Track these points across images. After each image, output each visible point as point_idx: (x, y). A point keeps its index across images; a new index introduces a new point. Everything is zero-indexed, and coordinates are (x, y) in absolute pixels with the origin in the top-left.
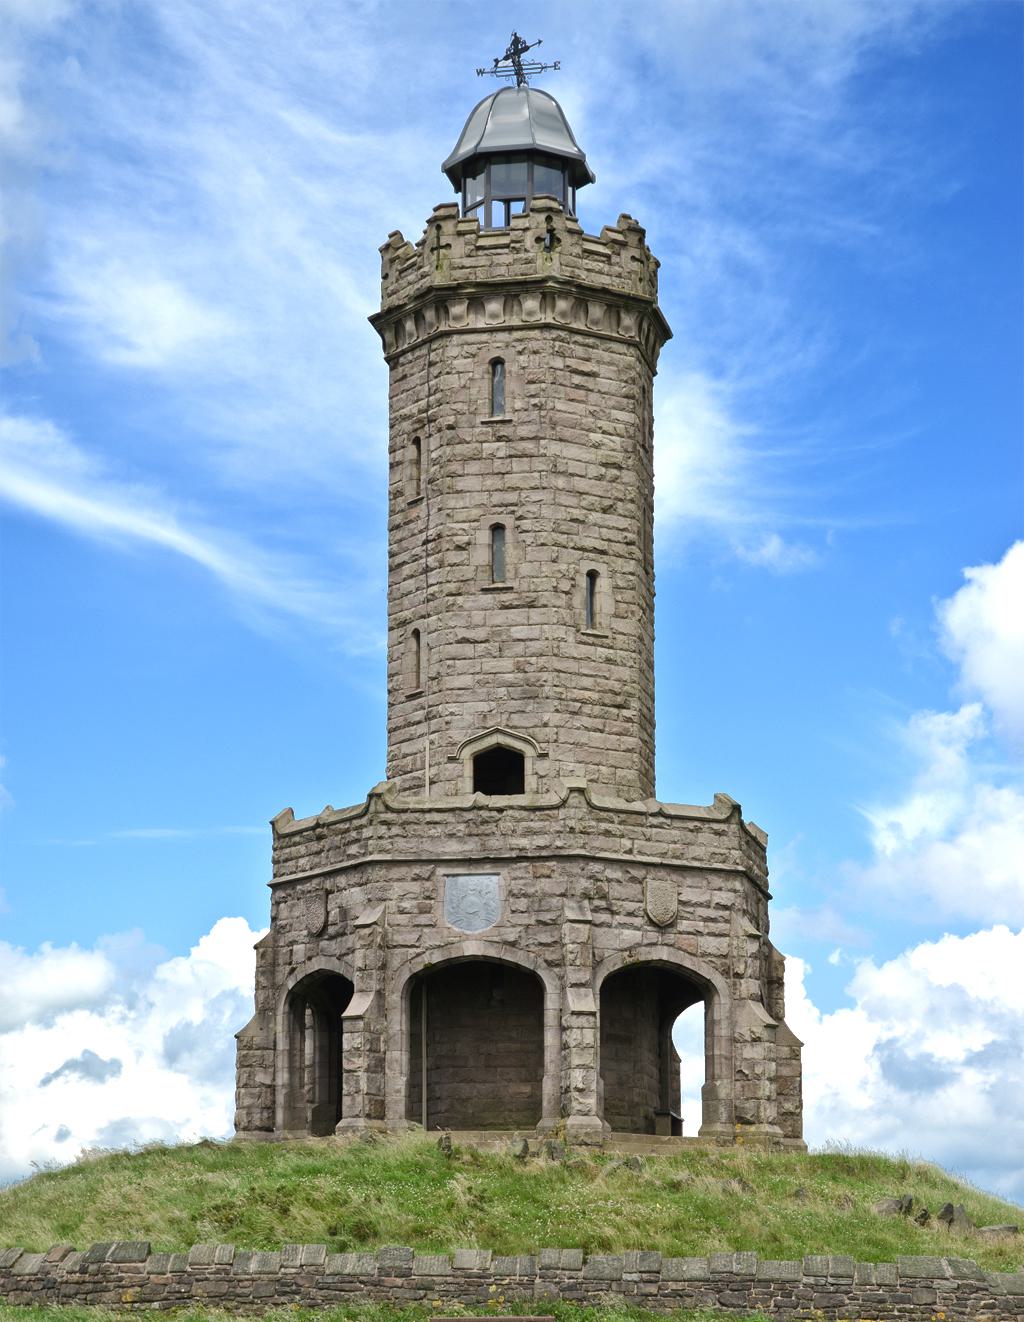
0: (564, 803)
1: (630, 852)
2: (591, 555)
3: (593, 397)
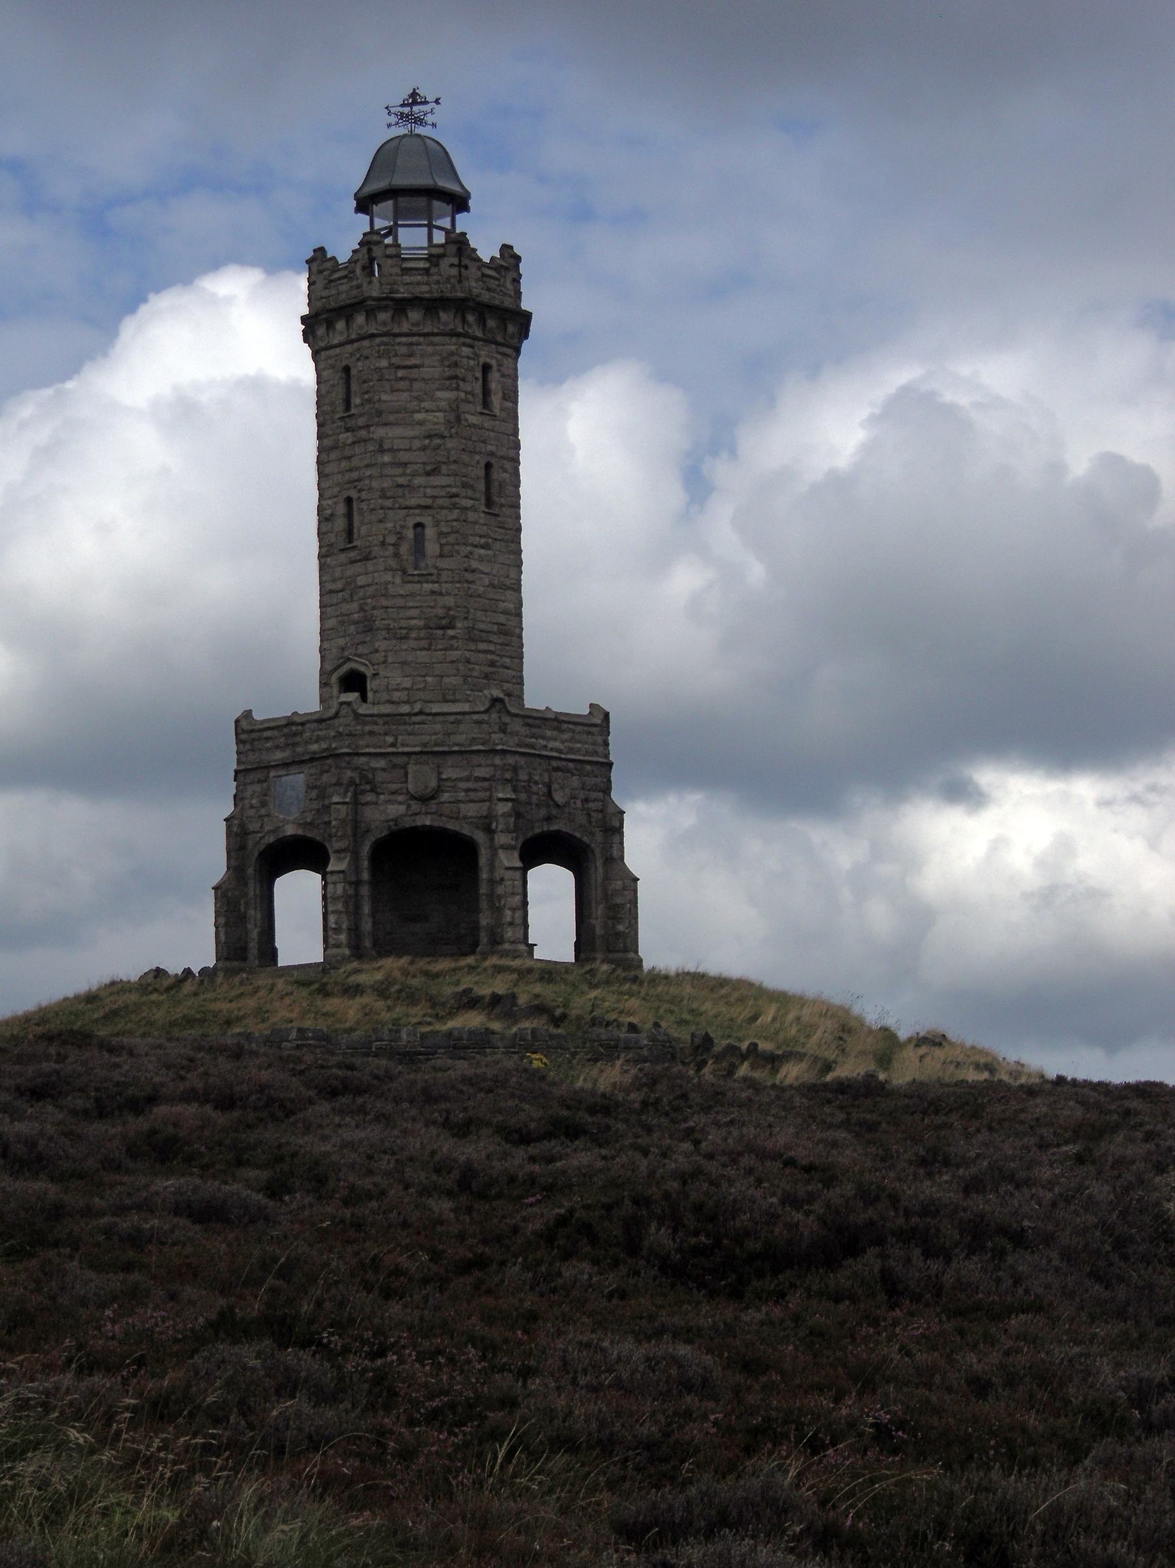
0: (336, 715)
1: (393, 745)
2: (417, 511)
3: (416, 385)
